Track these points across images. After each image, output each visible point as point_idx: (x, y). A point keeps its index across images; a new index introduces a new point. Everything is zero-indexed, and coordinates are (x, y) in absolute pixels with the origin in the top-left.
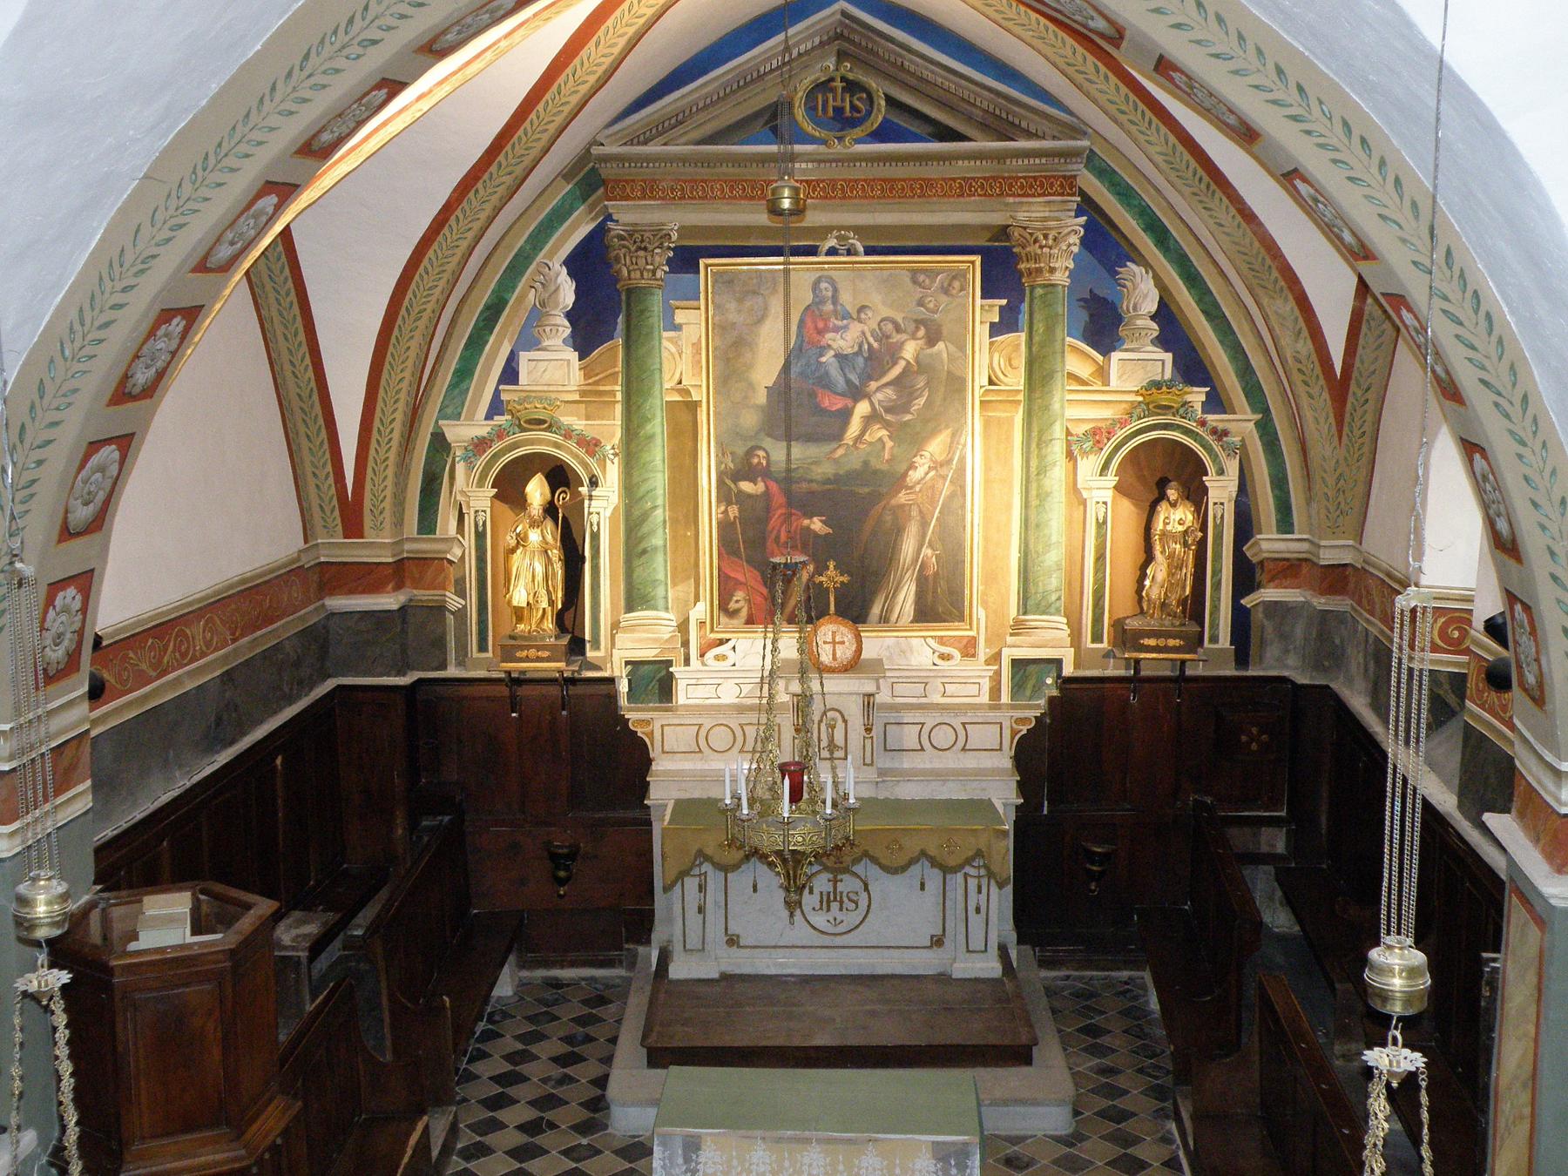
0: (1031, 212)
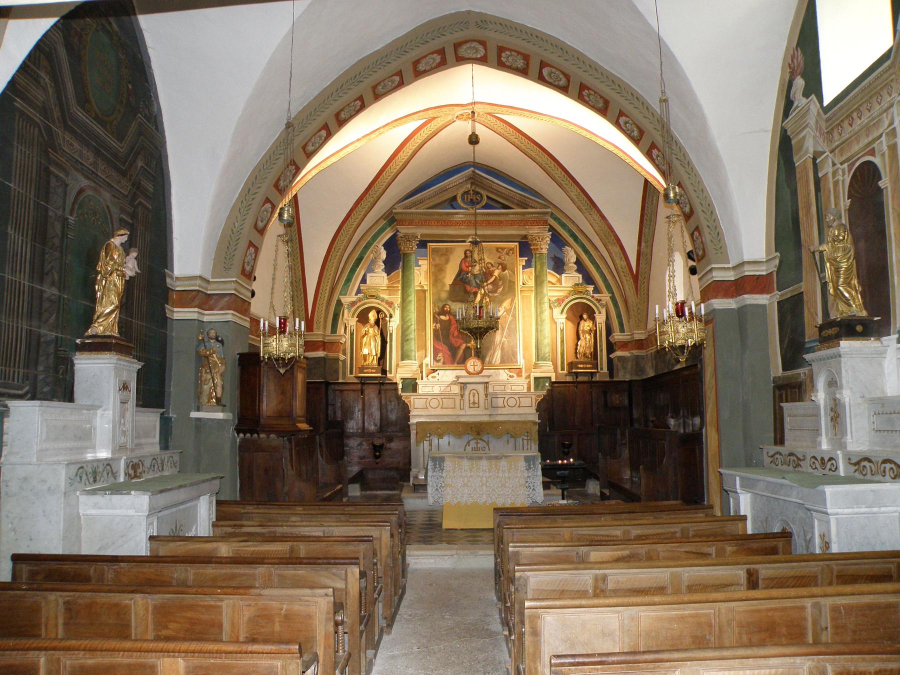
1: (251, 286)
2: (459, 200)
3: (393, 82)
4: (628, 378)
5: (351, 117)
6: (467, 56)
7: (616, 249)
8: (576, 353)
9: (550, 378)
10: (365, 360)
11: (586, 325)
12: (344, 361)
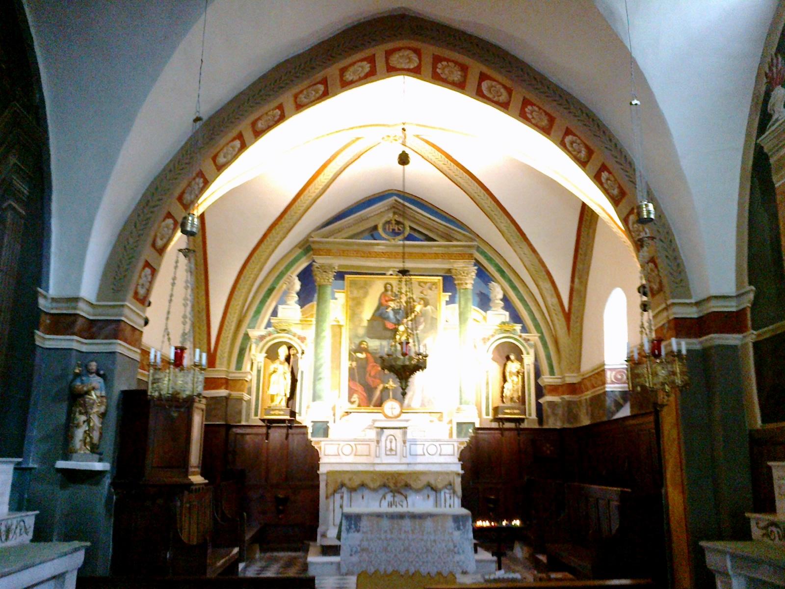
0: (458, 265)
1: (144, 311)
2: (380, 230)
3: (316, 91)
4: (558, 425)
5: (269, 128)
6: (398, 66)
7: (546, 285)
8: (502, 397)
9: (474, 424)
10: (272, 400)
11: (513, 366)
12: (249, 402)
